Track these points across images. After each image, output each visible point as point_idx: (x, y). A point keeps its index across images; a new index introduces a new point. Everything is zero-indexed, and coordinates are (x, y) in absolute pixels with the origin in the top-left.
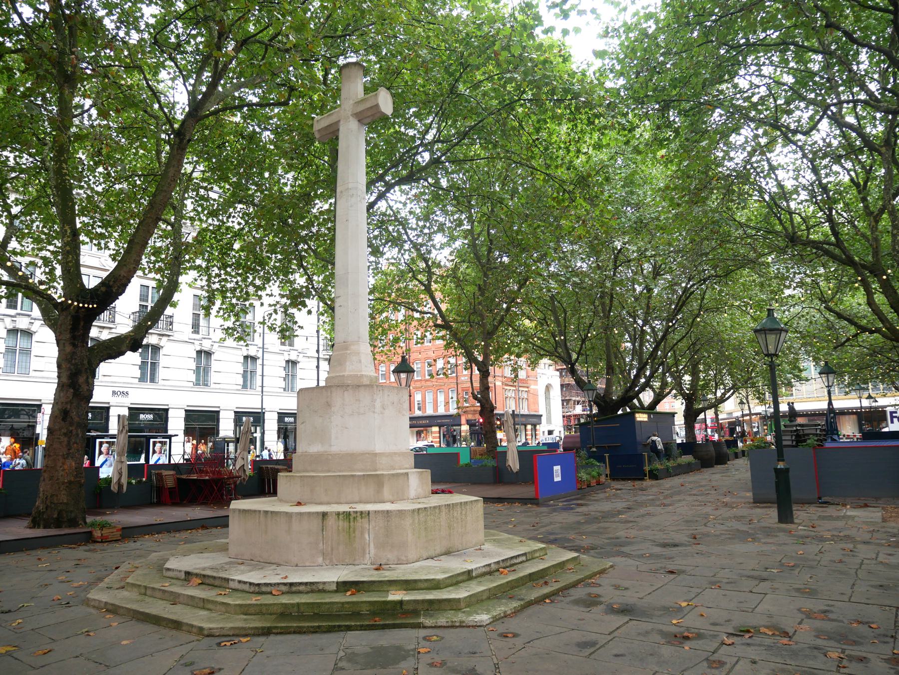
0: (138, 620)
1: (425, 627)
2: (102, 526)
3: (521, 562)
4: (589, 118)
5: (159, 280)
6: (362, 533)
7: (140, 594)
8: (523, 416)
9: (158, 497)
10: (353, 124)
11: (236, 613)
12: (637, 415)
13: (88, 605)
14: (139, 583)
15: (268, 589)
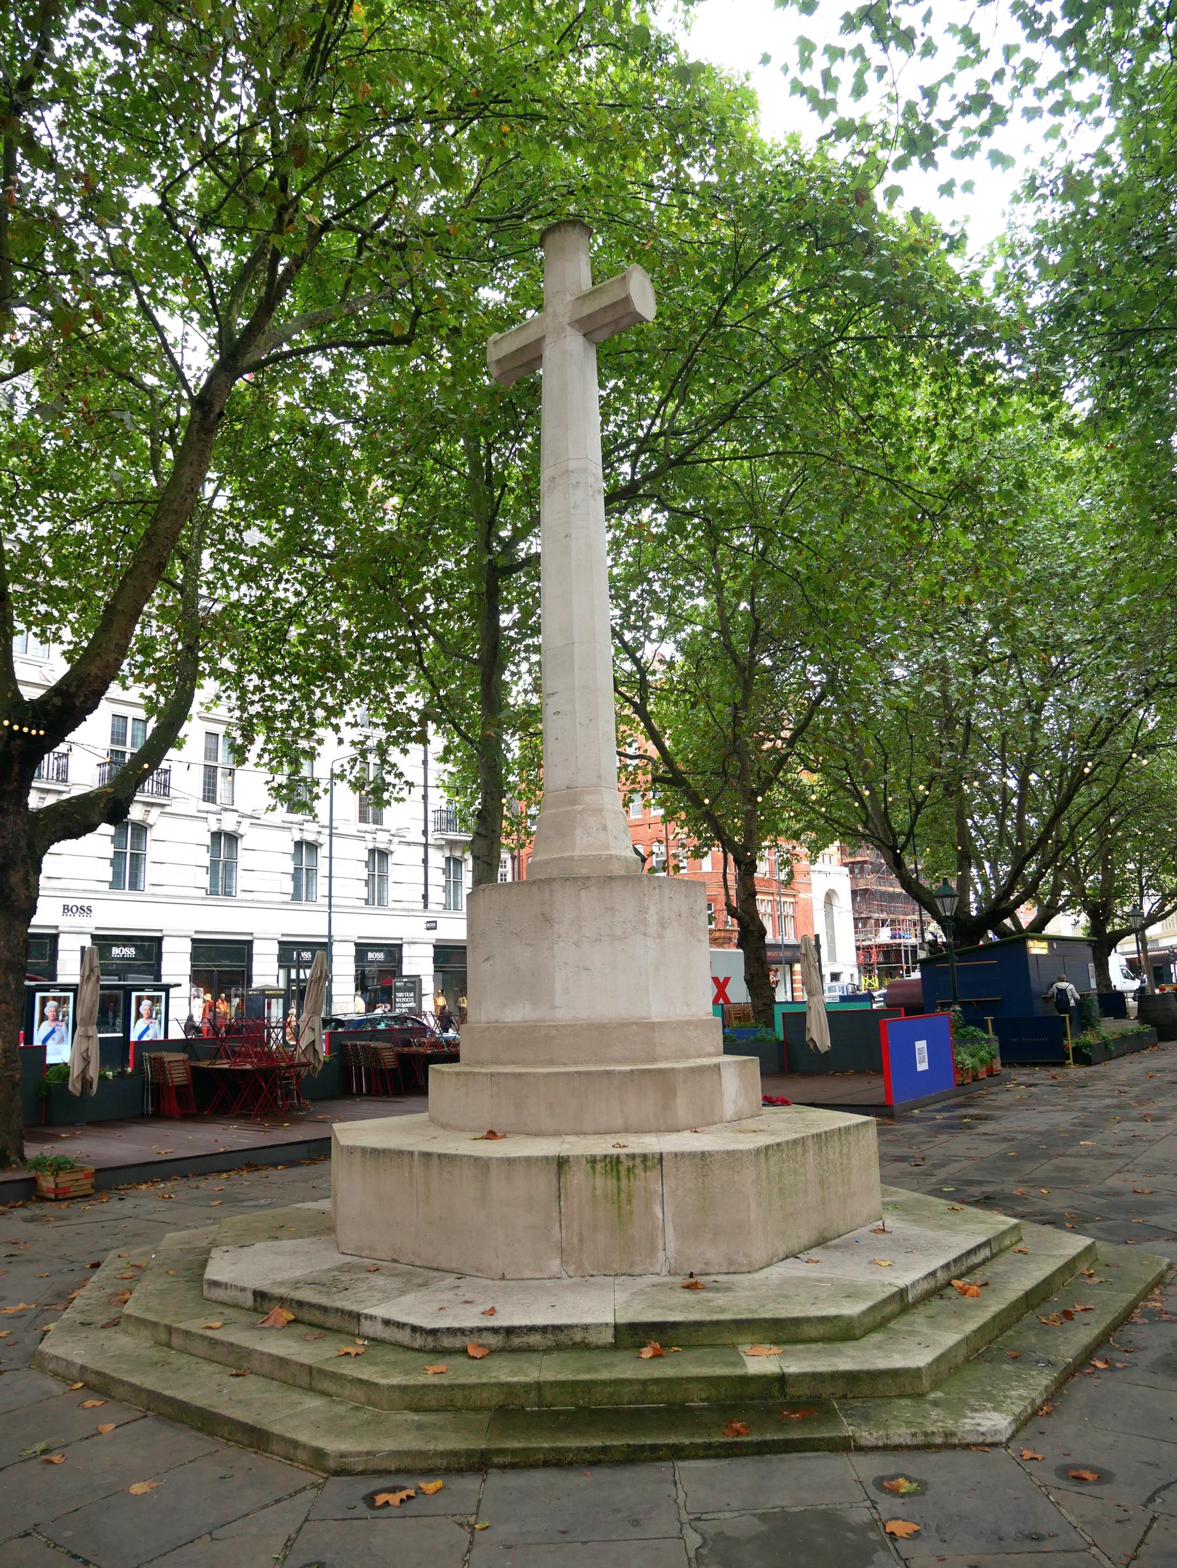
0: (161, 1416)
1: (861, 1449)
2: (58, 1167)
3: (984, 1262)
4: (974, 371)
5: (150, 698)
6: (648, 1205)
7: (158, 1343)
8: (787, 946)
9: (156, 1103)
10: (575, 343)
11: (394, 1408)
12: (1030, 943)
13: (42, 1370)
14: (152, 1317)
15: (457, 1342)
